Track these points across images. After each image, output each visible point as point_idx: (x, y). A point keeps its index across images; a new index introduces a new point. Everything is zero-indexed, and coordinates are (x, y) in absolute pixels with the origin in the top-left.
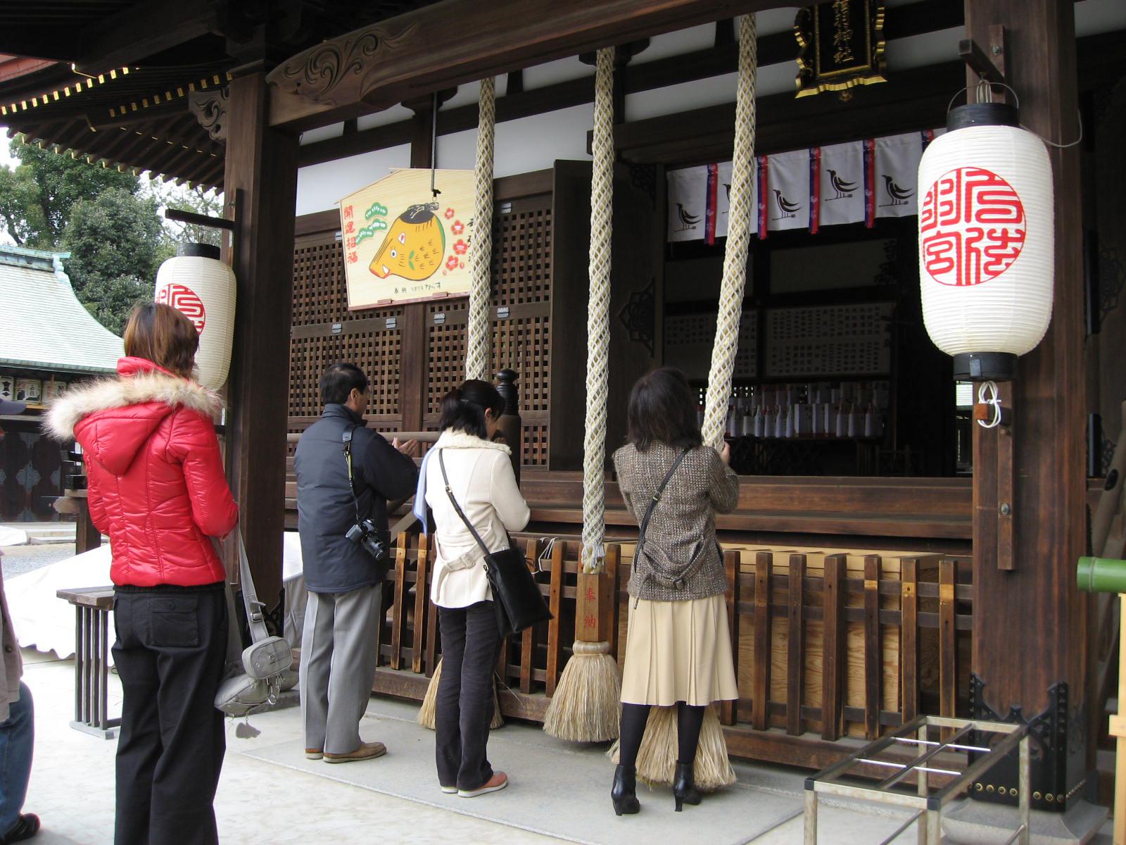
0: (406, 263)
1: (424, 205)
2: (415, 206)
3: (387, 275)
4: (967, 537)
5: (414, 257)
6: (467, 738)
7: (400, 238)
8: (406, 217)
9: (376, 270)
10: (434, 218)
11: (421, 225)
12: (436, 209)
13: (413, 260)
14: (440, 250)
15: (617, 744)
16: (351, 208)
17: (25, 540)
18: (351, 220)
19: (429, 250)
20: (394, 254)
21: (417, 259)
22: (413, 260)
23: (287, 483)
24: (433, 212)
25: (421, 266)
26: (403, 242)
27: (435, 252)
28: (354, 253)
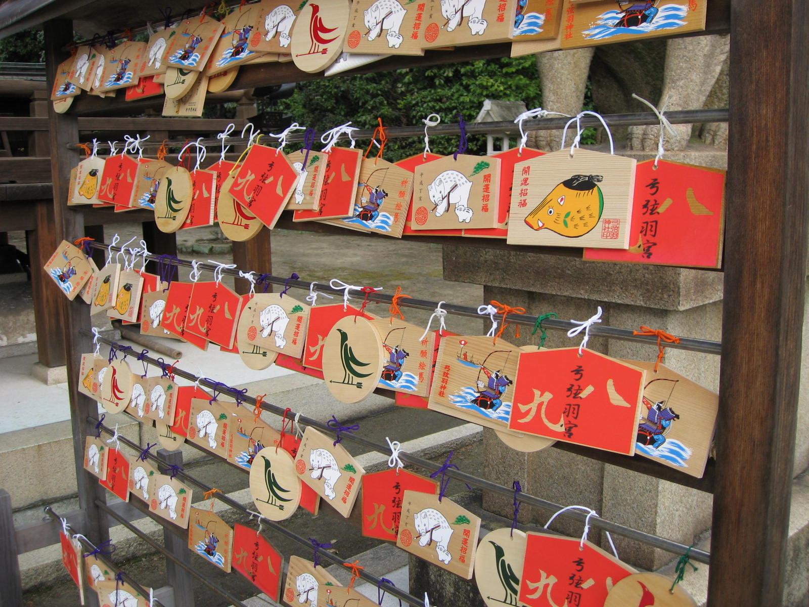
0: (561, 220)
1: (589, 177)
2: (579, 176)
3: (540, 228)
4: (482, 529)
5: (570, 217)
6: (33, 187)
7: (559, 200)
8: (568, 184)
9: (531, 223)
10: (596, 188)
11: (582, 192)
12: (599, 181)
13: (568, 220)
14: (596, 215)
15: (275, 574)
16: (529, 168)
17: (217, 398)
18: (527, 176)
19: (584, 213)
20: (551, 212)
21: (572, 219)
22: (568, 220)
23: (33, 337)
24: (596, 183)
25: (575, 225)
26: (562, 203)
27: (591, 216)
28: (525, 201)
